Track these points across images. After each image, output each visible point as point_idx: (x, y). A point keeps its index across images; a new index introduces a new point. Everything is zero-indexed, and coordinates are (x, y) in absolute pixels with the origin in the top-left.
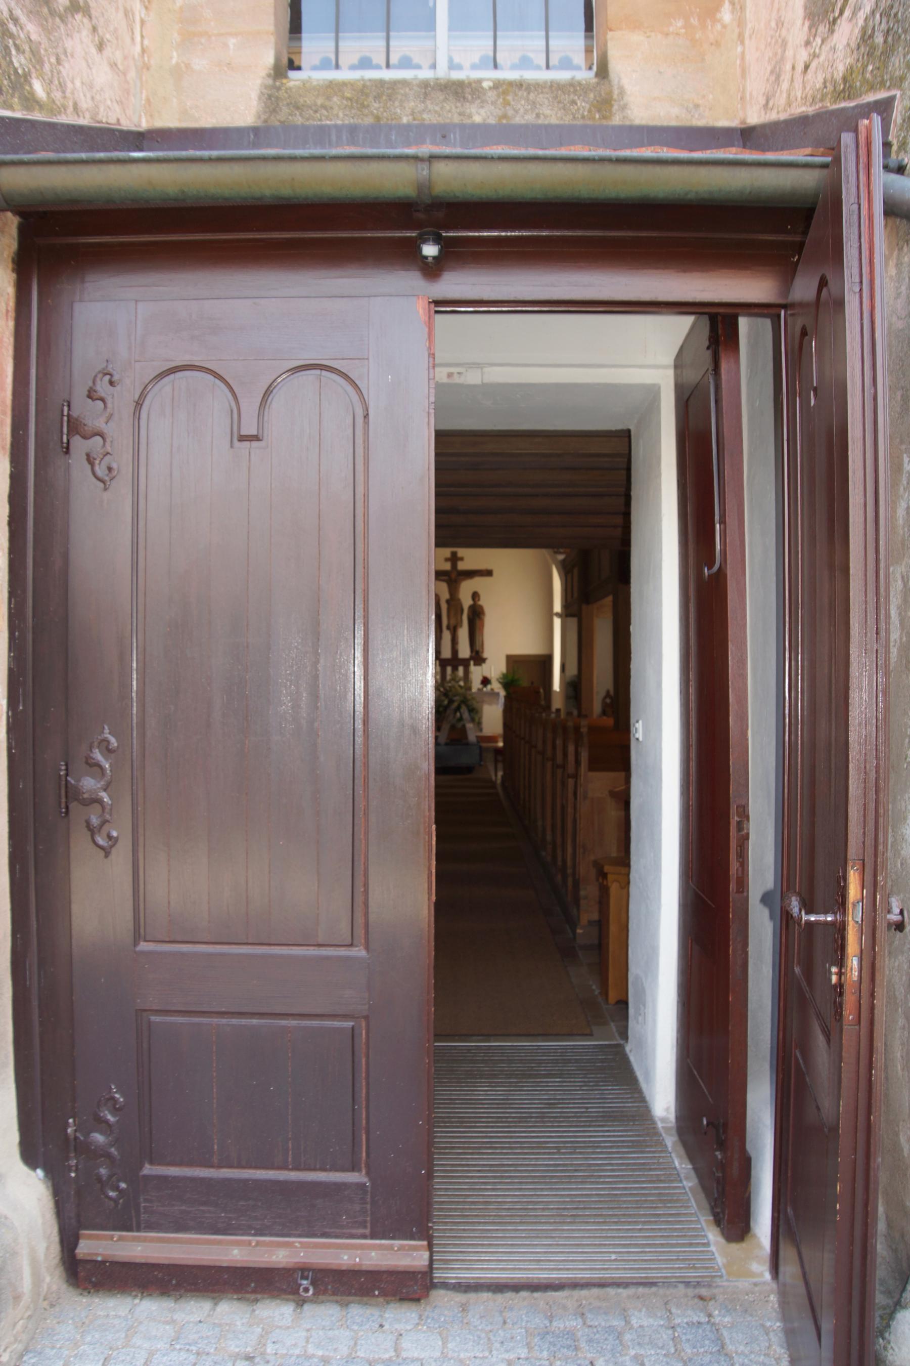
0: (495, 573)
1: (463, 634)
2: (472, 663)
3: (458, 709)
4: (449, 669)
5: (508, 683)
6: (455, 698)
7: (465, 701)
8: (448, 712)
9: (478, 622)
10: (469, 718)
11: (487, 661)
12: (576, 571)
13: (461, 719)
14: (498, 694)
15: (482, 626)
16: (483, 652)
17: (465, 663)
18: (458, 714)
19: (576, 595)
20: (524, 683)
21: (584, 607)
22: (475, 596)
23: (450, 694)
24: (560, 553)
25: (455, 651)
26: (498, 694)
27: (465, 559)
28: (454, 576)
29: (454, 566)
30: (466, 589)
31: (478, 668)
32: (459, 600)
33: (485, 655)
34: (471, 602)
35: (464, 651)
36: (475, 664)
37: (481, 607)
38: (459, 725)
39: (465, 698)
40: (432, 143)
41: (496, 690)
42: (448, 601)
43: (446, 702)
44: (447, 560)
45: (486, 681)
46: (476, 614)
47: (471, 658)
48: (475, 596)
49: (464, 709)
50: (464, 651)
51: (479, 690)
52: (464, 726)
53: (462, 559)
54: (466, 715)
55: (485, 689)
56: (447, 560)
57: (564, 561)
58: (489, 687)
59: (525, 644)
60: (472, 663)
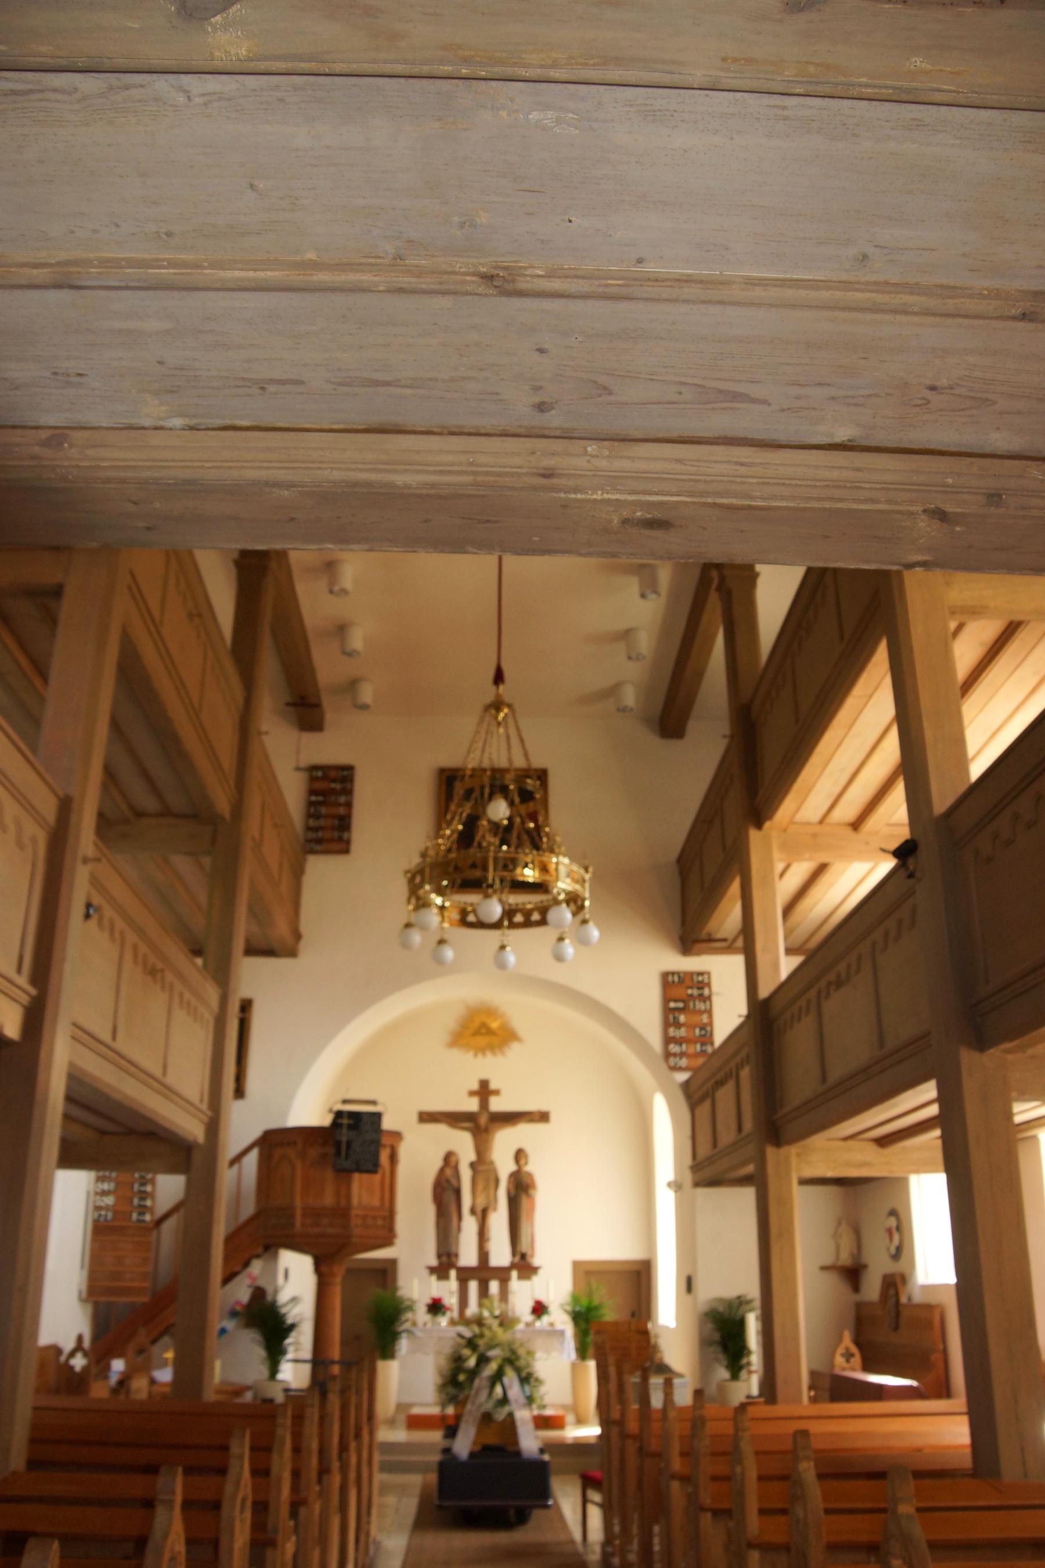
0: (553, 1117)
2: (514, 1274)
3: (498, 1377)
4: (473, 1286)
5: (583, 1318)
6: (491, 1353)
7: (511, 1360)
8: (477, 1382)
9: (524, 1201)
10: (522, 1400)
11: (541, 1272)
12: (745, 1073)
13: (504, 1401)
15: (532, 1209)
16: (532, 1256)
17: (503, 1275)
18: (498, 1390)
19: (748, 1125)
20: (610, 1313)
21: (770, 1151)
22: (520, 1155)
23: (481, 1342)
24: (681, 1069)
25: (483, 1255)
26: (562, 1333)
27: (504, 1092)
28: (483, 1120)
29: (484, 1104)
30: (504, 1144)
31: (525, 1284)
32: (492, 1163)
33: (536, 1261)
34: (513, 1167)
35: (501, 1255)
36: (521, 1277)
37: (530, 1175)
38: (501, 1415)
39: (513, 1352)
40: (388, 1238)
41: (559, 1326)
42: (473, 1165)
43: (472, 1362)
44: (472, 1093)
45: (539, 1309)
46: (521, 1187)
47: (513, 1266)
48: (520, 1155)
49: (510, 1378)
50: (501, 1255)
51: (528, 1325)
52: (511, 1415)
53: (497, 1092)
55: (538, 1324)
56: (472, 1093)
57: (686, 1086)
58: (545, 1319)
59: (614, 1247)
60: (514, 1274)
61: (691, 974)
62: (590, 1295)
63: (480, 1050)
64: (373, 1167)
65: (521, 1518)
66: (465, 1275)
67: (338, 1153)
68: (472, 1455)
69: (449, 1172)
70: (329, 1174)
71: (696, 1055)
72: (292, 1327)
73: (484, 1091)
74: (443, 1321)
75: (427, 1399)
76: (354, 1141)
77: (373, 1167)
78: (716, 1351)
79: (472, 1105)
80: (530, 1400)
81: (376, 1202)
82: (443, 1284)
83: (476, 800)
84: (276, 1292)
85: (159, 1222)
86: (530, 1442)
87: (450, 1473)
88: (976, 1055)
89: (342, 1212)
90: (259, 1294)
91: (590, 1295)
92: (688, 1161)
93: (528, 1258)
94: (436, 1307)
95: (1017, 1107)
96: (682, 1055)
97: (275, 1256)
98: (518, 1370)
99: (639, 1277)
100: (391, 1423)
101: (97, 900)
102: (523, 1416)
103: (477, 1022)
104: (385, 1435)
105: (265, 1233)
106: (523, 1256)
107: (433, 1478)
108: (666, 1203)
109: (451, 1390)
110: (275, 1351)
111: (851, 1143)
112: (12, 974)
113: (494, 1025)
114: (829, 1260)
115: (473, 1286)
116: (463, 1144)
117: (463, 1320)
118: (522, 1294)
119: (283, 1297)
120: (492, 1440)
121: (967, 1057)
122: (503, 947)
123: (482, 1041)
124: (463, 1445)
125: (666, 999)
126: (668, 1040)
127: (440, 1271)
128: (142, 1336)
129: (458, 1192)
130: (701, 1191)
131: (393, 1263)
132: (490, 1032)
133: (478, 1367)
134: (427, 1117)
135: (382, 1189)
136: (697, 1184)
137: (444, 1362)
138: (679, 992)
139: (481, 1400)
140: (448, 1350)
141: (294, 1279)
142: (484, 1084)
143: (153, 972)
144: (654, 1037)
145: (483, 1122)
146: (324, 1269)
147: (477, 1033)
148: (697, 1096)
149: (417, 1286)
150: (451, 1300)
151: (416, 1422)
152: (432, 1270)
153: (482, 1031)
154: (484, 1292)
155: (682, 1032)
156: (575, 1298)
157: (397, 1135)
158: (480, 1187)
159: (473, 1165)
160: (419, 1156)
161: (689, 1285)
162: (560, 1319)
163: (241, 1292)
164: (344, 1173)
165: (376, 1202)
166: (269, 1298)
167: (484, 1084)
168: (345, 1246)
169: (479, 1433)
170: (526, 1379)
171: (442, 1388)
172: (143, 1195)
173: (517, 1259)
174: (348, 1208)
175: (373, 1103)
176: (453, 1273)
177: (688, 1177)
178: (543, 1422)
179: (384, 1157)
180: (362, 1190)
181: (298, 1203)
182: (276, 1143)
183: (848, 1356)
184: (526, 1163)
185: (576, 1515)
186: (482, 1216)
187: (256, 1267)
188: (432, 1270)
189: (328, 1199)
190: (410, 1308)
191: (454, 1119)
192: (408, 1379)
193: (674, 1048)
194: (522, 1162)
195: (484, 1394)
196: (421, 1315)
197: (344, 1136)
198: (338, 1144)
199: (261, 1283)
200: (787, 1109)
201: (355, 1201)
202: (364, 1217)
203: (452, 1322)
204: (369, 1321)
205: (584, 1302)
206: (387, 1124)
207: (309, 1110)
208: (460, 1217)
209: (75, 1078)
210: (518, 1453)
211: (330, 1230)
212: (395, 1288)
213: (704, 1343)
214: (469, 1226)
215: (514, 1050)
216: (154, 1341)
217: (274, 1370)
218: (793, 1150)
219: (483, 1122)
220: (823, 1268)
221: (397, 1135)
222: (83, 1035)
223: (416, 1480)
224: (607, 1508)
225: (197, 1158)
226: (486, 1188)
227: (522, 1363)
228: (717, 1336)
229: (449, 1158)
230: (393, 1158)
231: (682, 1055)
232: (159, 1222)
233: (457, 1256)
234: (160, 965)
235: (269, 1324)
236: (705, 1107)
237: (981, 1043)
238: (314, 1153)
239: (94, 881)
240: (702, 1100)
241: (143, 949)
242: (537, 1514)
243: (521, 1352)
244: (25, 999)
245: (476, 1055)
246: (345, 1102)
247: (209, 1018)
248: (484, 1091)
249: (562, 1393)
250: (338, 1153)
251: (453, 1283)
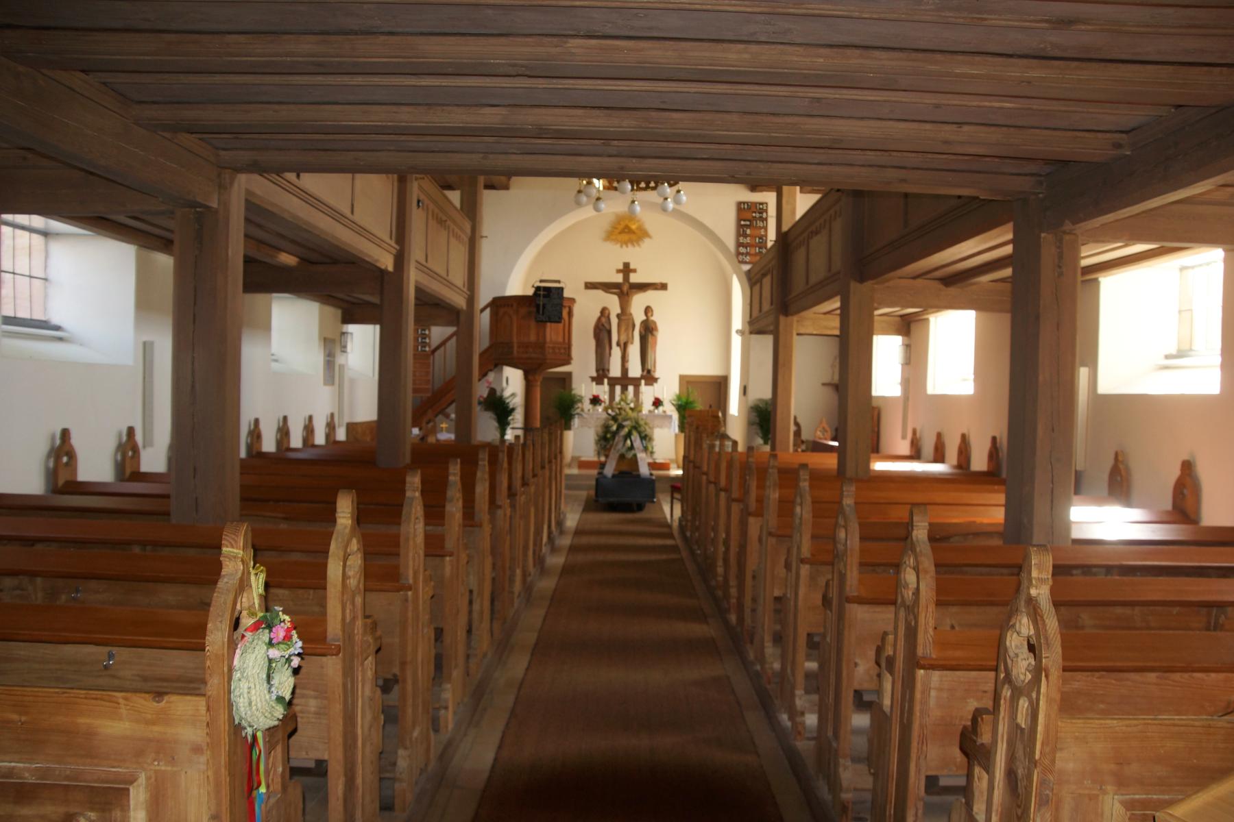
1: (634, 350)
2: (643, 382)
3: (629, 435)
4: (618, 389)
5: (683, 408)
7: (636, 427)
9: (650, 338)
13: (632, 448)
14: (671, 417)
15: (655, 343)
17: (636, 382)
18: (629, 442)
20: (699, 406)
21: (782, 319)
22: (648, 310)
24: (746, 263)
25: (625, 370)
26: (671, 417)
28: (625, 288)
29: (626, 278)
30: (638, 303)
33: (657, 375)
34: (644, 318)
35: (635, 370)
37: (654, 323)
39: (637, 423)
40: (567, 360)
41: (669, 413)
42: (618, 316)
43: (614, 428)
44: (619, 271)
45: (657, 403)
46: (648, 330)
47: (642, 377)
48: (648, 310)
50: (635, 370)
52: (635, 455)
53: (634, 271)
54: (637, 443)
56: (619, 271)
57: (748, 273)
58: (661, 408)
59: (705, 367)
60: (643, 382)
61: (755, 204)
62: (688, 395)
63: (625, 243)
64: (559, 319)
65: (640, 507)
66: (613, 382)
67: (538, 311)
68: (614, 476)
69: (603, 320)
70: (533, 324)
71: (756, 254)
72: (513, 410)
73: (626, 270)
74: (600, 409)
75: (589, 452)
76: (547, 303)
77: (559, 319)
78: (756, 428)
79: (619, 278)
80: (646, 449)
81: (561, 340)
82: (600, 387)
83: (562, 533)
84: (503, 390)
85: (434, 351)
86: (644, 470)
87: (601, 485)
88: (858, 285)
89: (541, 345)
90: (492, 391)
91: (688, 395)
92: (748, 319)
94: (595, 401)
95: (1085, 251)
96: (747, 254)
97: (501, 370)
98: (639, 433)
99: (721, 385)
100: (570, 466)
101: (422, 197)
102: (641, 456)
103: (621, 227)
104: (567, 471)
105: (497, 358)
106: (649, 371)
107: (593, 492)
108: (736, 342)
109: (603, 443)
110: (503, 423)
111: (828, 316)
112: (388, 240)
113: (633, 227)
114: (827, 380)
115: (618, 389)
116: (612, 303)
117: (611, 406)
118: (648, 393)
119: (507, 394)
120: (624, 468)
121: (854, 285)
122: (633, 202)
123: (625, 237)
124: (609, 471)
125: (739, 219)
126: (739, 245)
127: (598, 380)
128: (430, 413)
129: (609, 332)
130: (754, 337)
131: (569, 374)
132: (631, 231)
133: (620, 431)
134: (590, 286)
136: (751, 333)
137: (600, 430)
138: (748, 215)
139: (619, 446)
140: (601, 422)
141: (512, 382)
142: (626, 265)
143: (441, 222)
144: (731, 243)
145: (625, 289)
146: (531, 378)
147: (622, 232)
148: (752, 280)
149: (584, 388)
150: (605, 397)
151: (583, 465)
152: (593, 379)
153: (626, 231)
154: (624, 389)
155: (748, 240)
156: (679, 398)
157: (573, 300)
158: (623, 329)
159: (618, 316)
160: (586, 309)
161: (744, 390)
162: (669, 409)
163: (481, 390)
164: (541, 322)
165: (561, 340)
166: (498, 394)
167: (626, 265)
168: (544, 367)
169: (617, 465)
170: (645, 438)
171: (597, 442)
172: (424, 336)
174: (545, 342)
176: (606, 381)
177: (747, 328)
178: (654, 466)
179: (565, 313)
180: (552, 332)
181: (515, 340)
182: (500, 305)
183: (824, 430)
185: (670, 510)
186: (624, 347)
187: (491, 376)
188: (593, 379)
189: (533, 338)
190: (580, 401)
191: (607, 287)
192: (579, 441)
193: (742, 250)
195: (621, 445)
196: (587, 405)
197: (541, 301)
198: (538, 306)
199: (493, 386)
200: (794, 294)
201: (548, 339)
202: (553, 348)
203: (606, 409)
204: (558, 408)
205: (684, 400)
206: (566, 294)
207: (518, 285)
208: (611, 348)
209: (419, 290)
210: (639, 476)
211: (534, 355)
212: (571, 389)
213: (750, 424)
214: (616, 353)
215: (647, 243)
216: (436, 416)
217: (503, 434)
218: (795, 318)
219: (625, 289)
220: (824, 384)
221: (573, 300)
222: (422, 267)
223: (583, 494)
224: (682, 501)
225: (462, 318)
226: (627, 329)
227: (642, 429)
228: (757, 420)
230: (570, 314)
231: (747, 254)
232: (434, 351)
234: (444, 218)
235: (501, 410)
236: (757, 288)
237: (862, 280)
238: (523, 311)
239: (420, 187)
240: (755, 283)
241: (436, 210)
242: (648, 505)
243: (642, 423)
244: (394, 252)
246: (541, 281)
247: (466, 240)
248: (626, 270)
249: (666, 445)
250: (538, 311)
251: (606, 387)
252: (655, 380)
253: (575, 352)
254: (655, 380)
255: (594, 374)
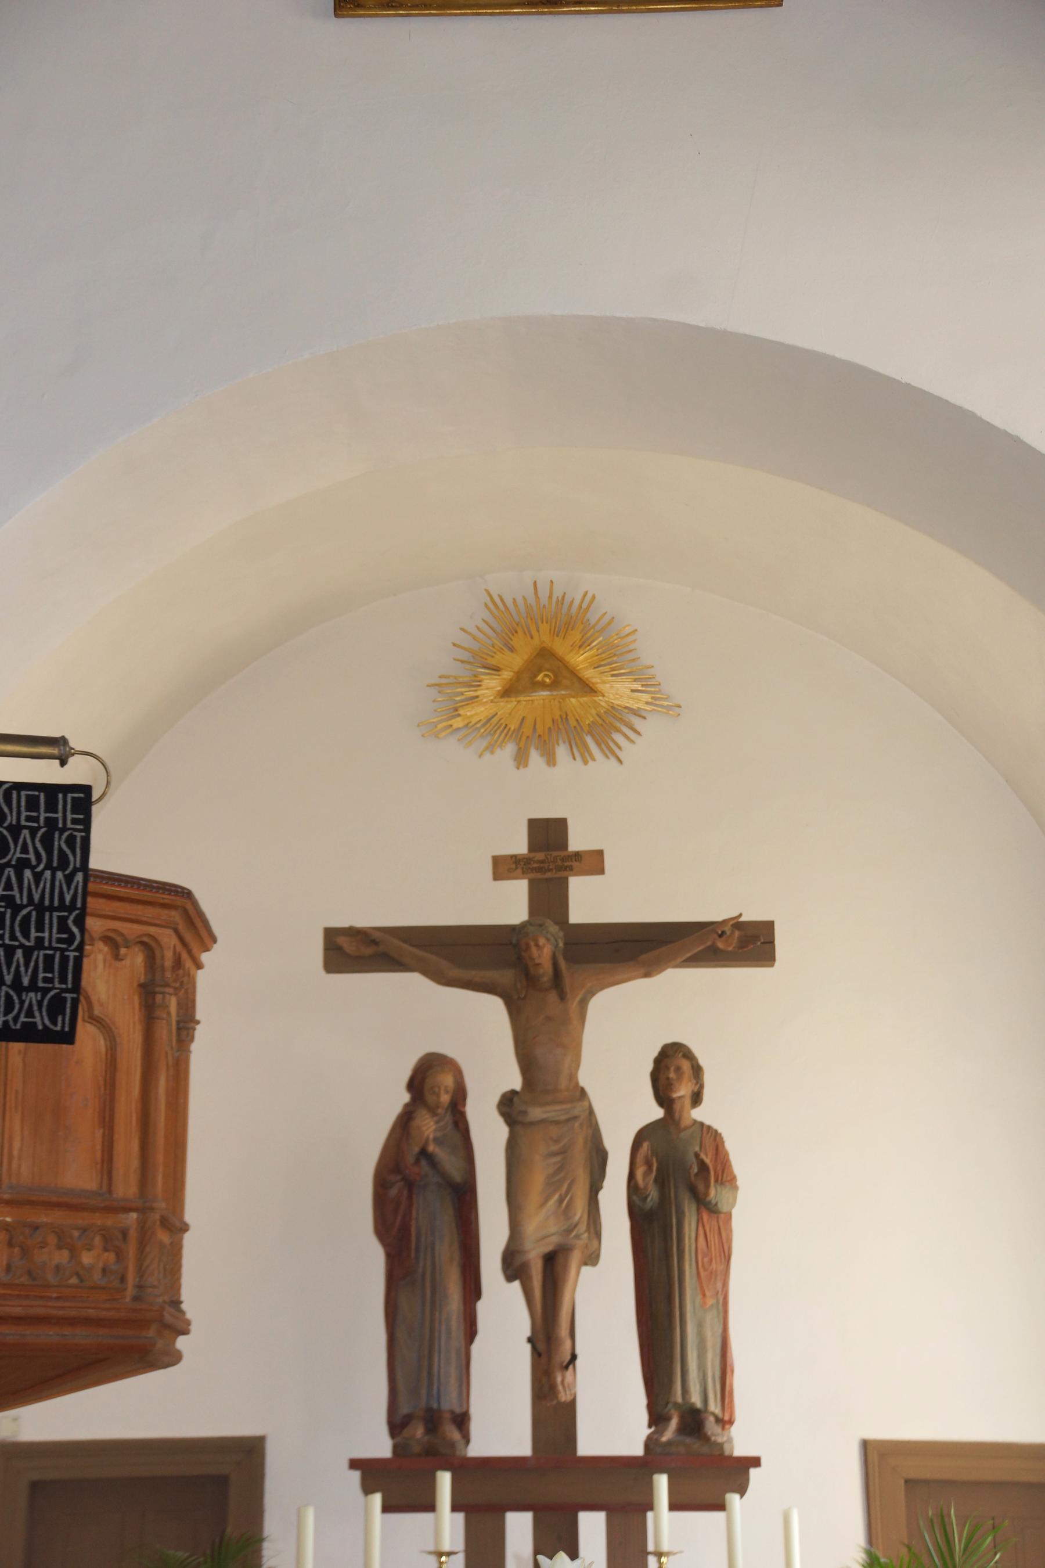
2: (662, 1483)
16: (725, 1422)
17: (620, 1490)
22: (673, 1070)
28: (544, 953)
29: (549, 899)
30: (618, 1034)
33: (741, 1442)
37: (712, 1138)
42: (509, 1106)
44: (504, 867)
46: (680, 1184)
48: (673, 1070)
50: (613, 1419)
53: (593, 863)
56: (504, 867)
60: (662, 1483)
73: (549, 856)
79: (510, 905)
81: (78, 1175)
93: (711, 1427)
106: (693, 1422)
113: (579, 660)
116: (479, 1037)
134: (355, 950)
135: (107, 1119)
142: (548, 834)
145: (542, 961)
152: (371, 1473)
159: (509, 1106)
167: (548, 834)
173: (669, 1433)
175: (58, 748)
176: (445, 1480)
179: (107, 982)
184: (697, 1099)
186: (547, 1282)
188: (371, 1473)
194: (683, 1091)
206: (115, 846)
214: (504, 1312)
219: (542, 961)
229: (434, 1087)
233: (462, 1421)
245: (521, 759)
248: (549, 856)
252: (737, 1472)
253: (208, 1275)
254: (737, 1472)
255: (382, 1447)
